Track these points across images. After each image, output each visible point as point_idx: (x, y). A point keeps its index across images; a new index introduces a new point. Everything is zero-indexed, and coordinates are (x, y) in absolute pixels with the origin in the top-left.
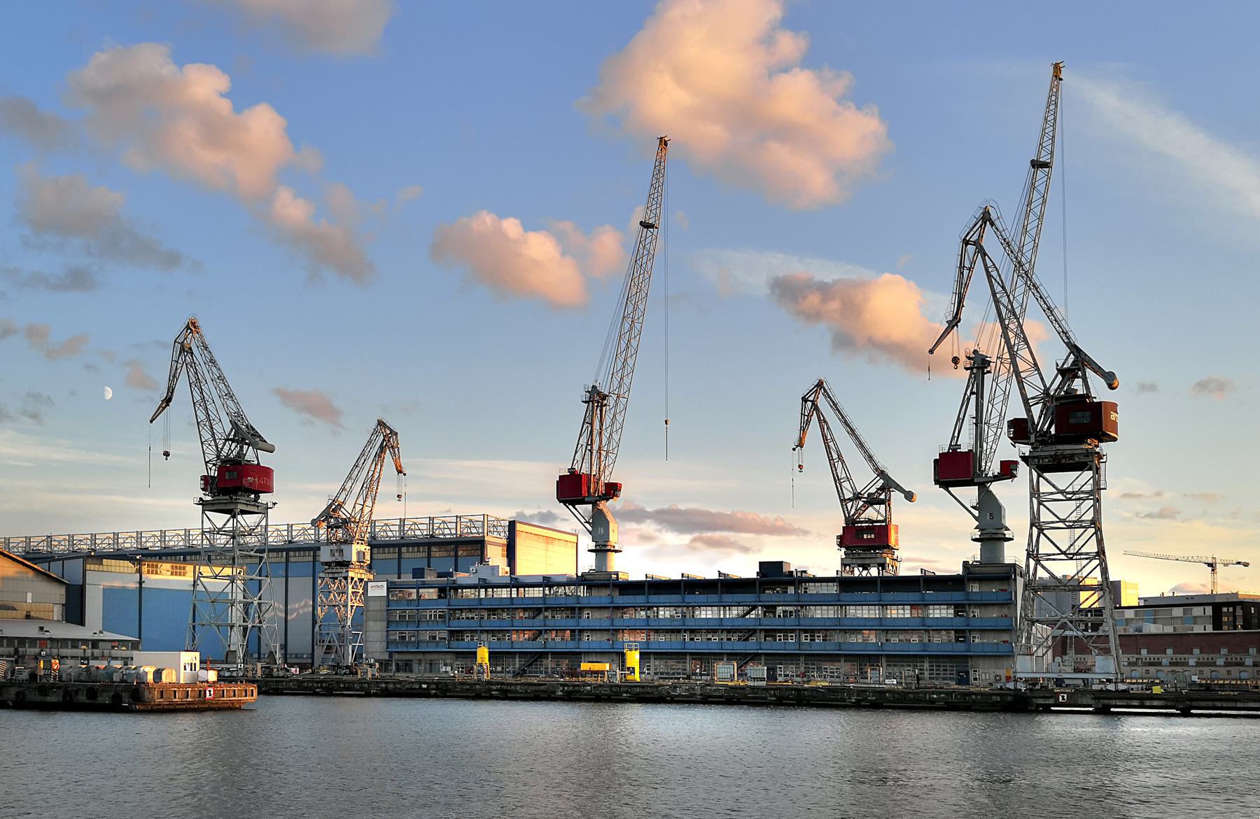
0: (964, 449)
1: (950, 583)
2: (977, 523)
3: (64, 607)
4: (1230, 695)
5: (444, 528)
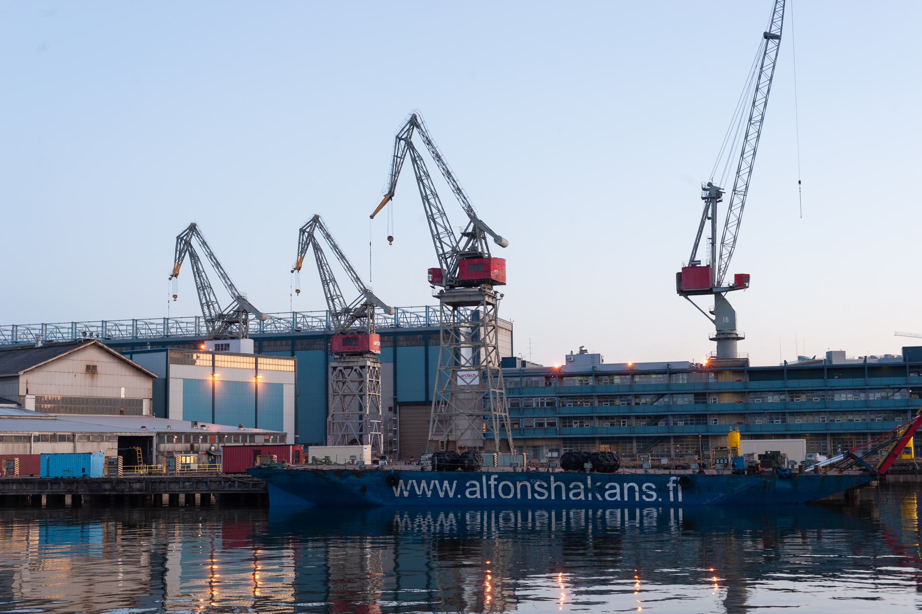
0: (703, 264)
3: (152, 402)
5: (56, 333)
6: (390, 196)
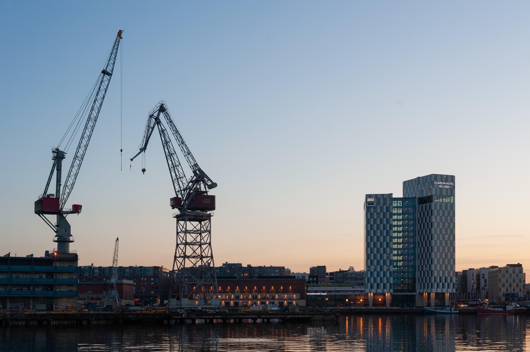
2: (56, 234)
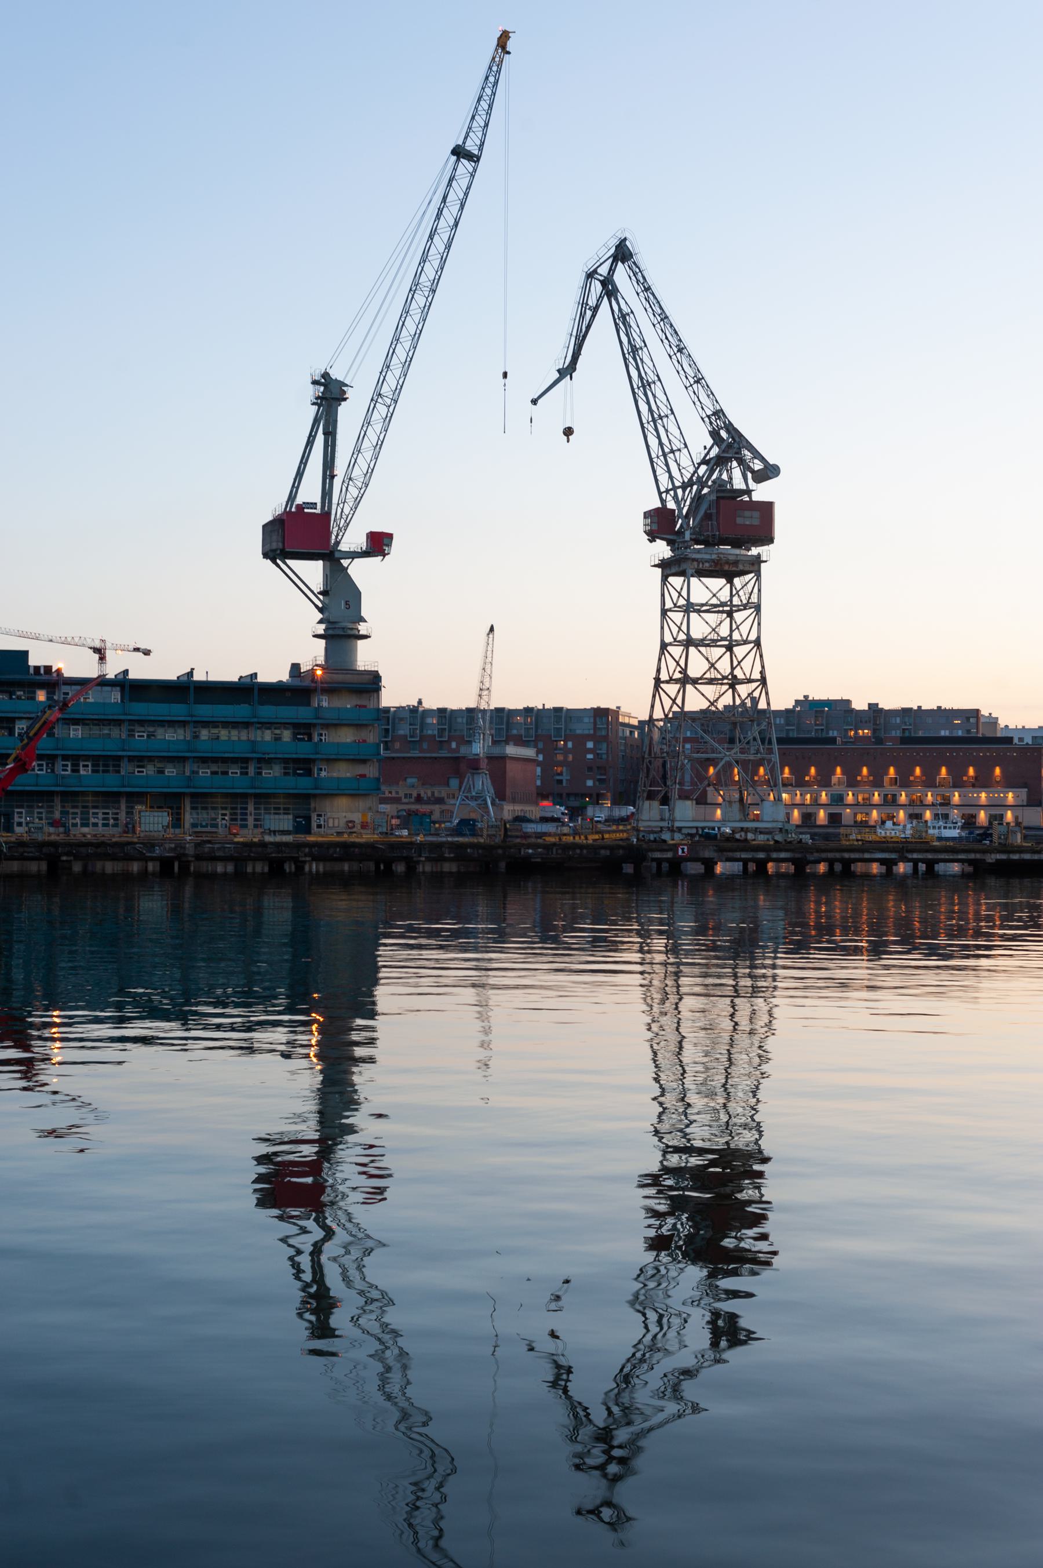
1: (288, 694)
4: (853, 845)
6: (568, 371)
